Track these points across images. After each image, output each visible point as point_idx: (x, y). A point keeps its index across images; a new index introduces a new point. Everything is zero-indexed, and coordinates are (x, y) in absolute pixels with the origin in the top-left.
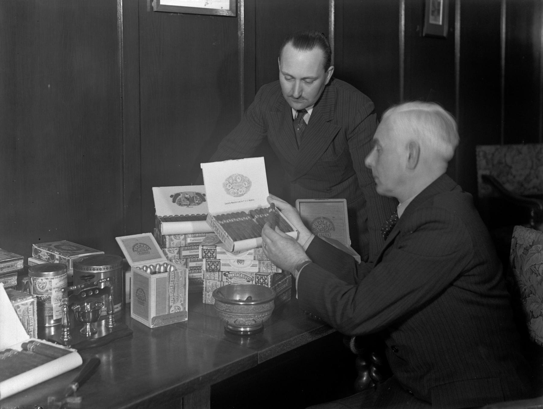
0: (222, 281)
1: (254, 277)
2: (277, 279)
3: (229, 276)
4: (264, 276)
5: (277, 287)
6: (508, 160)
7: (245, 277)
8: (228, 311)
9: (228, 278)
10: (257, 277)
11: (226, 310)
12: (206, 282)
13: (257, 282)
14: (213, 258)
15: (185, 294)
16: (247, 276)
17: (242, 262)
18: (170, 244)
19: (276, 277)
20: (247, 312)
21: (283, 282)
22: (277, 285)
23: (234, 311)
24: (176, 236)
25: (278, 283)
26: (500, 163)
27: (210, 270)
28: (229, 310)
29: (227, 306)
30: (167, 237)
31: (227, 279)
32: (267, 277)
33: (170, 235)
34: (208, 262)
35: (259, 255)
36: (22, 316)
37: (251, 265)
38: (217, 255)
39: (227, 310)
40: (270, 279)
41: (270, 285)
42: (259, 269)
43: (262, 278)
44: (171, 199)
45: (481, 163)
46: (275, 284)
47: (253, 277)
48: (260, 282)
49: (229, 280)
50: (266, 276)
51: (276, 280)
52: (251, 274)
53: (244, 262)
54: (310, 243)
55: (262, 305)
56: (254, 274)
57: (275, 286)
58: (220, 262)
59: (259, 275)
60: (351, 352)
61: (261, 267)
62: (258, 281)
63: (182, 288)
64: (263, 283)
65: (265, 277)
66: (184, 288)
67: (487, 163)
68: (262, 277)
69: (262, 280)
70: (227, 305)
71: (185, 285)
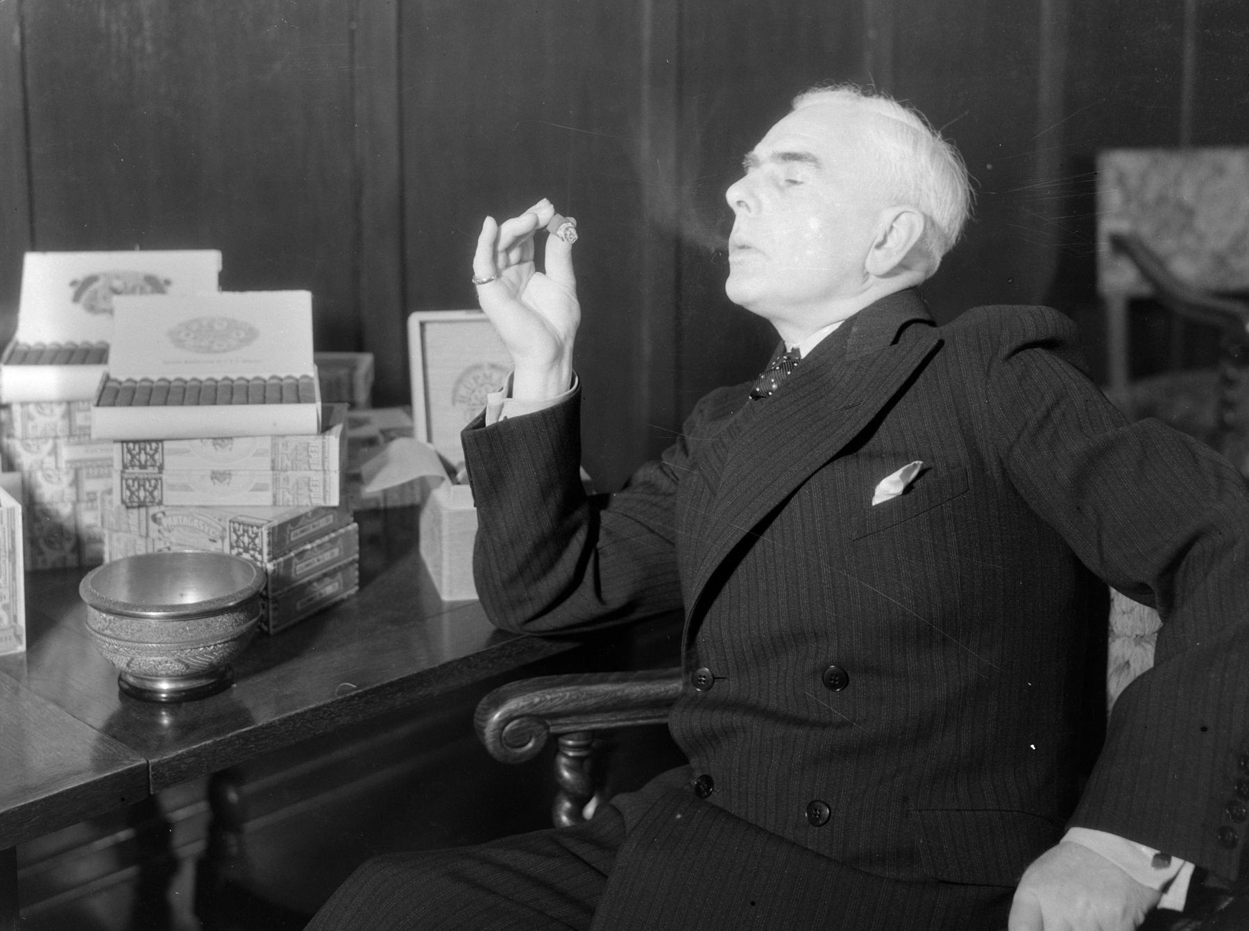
0: (147, 536)
1: (228, 529)
2: (296, 538)
3: (165, 525)
4: (252, 527)
5: (295, 560)
6: (1187, 194)
7: (204, 527)
8: (108, 632)
9: (161, 527)
10: (234, 528)
11: (103, 630)
12: (110, 538)
13: (234, 544)
14: (153, 466)
15: (14, 579)
16: (209, 525)
17: (225, 479)
18: (24, 427)
19: (291, 531)
20: (159, 638)
21: (320, 546)
22: (296, 555)
23: (123, 635)
24: (41, 408)
25: (301, 549)
26: (1161, 199)
27: (134, 502)
28: (111, 630)
29: (105, 619)
30: (16, 409)
31: (159, 531)
32: (260, 531)
33: (24, 404)
34: (127, 480)
35: (287, 454)
36: (293, 495)
37: (252, 486)
38: (165, 457)
39: (107, 629)
40: (269, 537)
41: (269, 554)
42: (274, 496)
43: (247, 532)
44: (71, 292)
45: (1111, 198)
46: (290, 551)
47: (224, 529)
48: (242, 545)
49: (166, 534)
50: (258, 527)
51: (292, 539)
52: (220, 520)
53: (230, 478)
54: (581, 423)
55: (207, 620)
56: (228, 520)
57: (286, 557)
58: (161, 479)
59: (239, 524)
60: (482, 747)
61: (281, 491)
62: (237, 541)
63: (5, 561)
64: (251, 546)
65: (255, 529)
66: (9, 560)
67: (1127, 200)
68: (246, 528)
69: (246, 540)
70: (104, 615)
71: (13, 551)
